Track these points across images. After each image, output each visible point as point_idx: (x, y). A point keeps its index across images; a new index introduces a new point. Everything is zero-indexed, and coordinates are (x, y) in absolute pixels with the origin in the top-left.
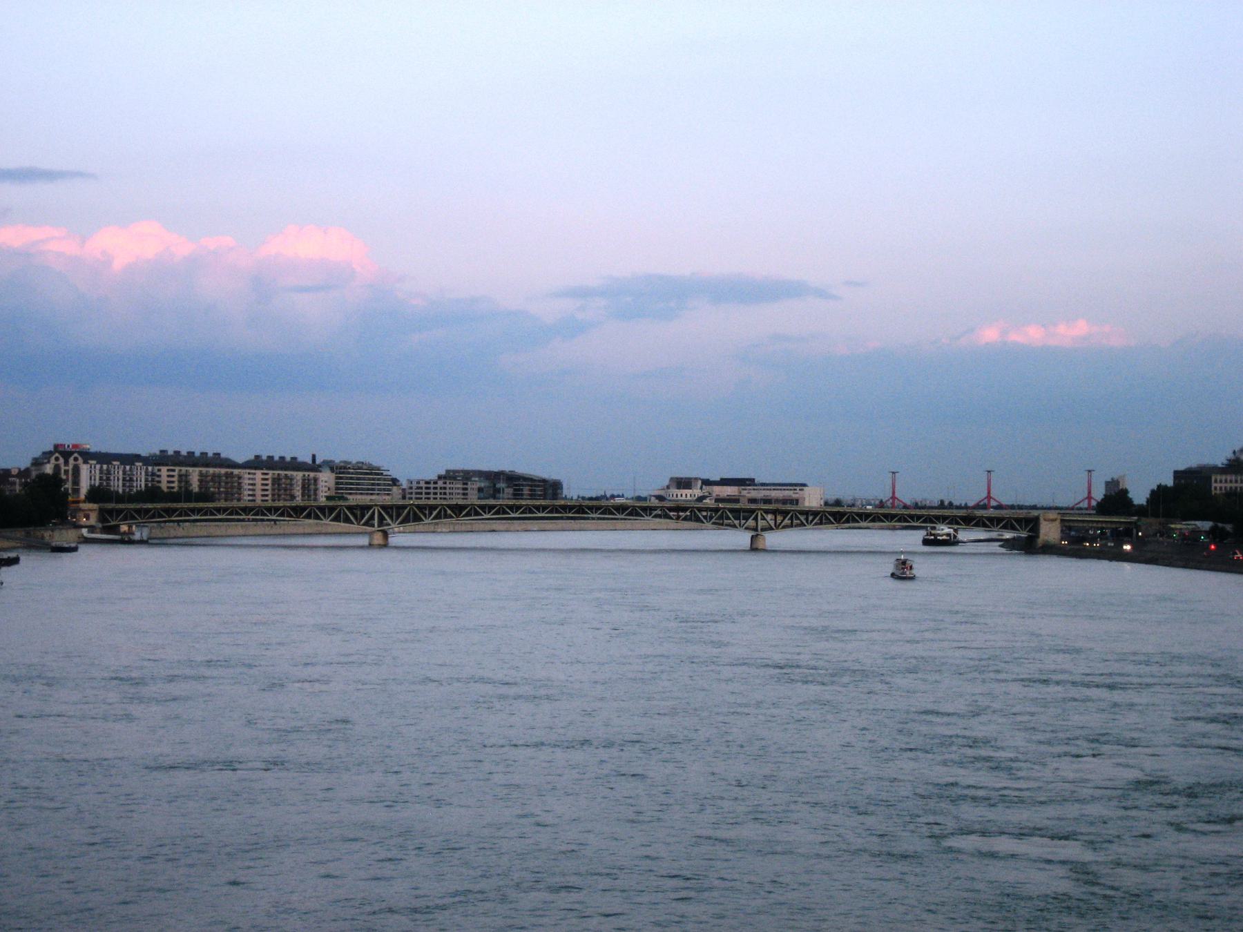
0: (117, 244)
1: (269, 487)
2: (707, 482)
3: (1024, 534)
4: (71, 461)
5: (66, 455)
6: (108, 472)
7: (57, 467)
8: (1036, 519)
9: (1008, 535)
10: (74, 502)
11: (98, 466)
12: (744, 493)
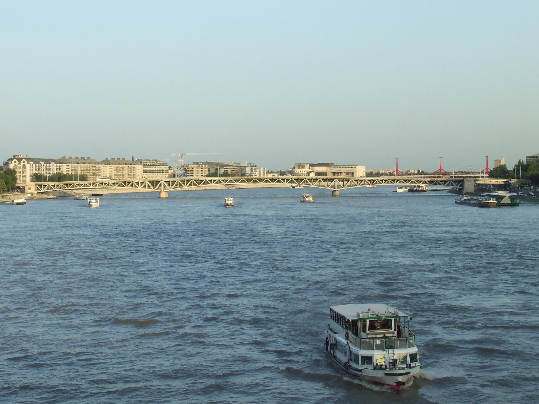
2: (311, 165)
3: (457, 187)
4: (22, 163)
5: (20, 160)
6: (39, 167)
8: (463, 180)
9: (449, 188)
10: (497, 173)
11: (34, 165)
12: (329, 169)
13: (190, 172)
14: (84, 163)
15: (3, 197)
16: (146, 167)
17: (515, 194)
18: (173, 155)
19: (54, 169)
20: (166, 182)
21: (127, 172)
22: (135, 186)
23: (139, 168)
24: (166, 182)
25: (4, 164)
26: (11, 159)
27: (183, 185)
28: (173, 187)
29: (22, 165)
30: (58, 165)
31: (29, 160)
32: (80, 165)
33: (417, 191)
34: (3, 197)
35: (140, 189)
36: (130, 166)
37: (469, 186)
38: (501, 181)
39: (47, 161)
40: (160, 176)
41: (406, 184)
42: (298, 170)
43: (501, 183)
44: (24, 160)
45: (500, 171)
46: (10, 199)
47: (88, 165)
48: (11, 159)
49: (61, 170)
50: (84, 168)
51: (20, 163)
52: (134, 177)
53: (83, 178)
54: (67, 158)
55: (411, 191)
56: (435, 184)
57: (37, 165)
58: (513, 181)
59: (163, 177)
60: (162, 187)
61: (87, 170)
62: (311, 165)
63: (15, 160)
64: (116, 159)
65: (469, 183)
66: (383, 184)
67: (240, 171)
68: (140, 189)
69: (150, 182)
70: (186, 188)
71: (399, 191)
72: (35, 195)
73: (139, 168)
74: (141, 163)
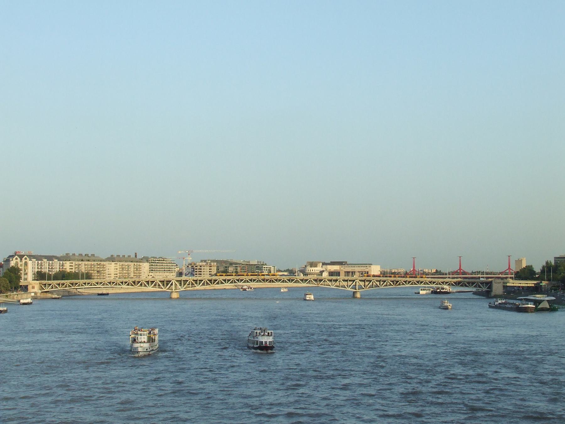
0: (564, 311)
1: (73, 267)
3: (485, 289)
4: (24, 260)
5: (21, 257)
6: (41, 264)
7: (17, 263)
8: (491, 282)
9: (474, 290)
11: (36, 262)
12: (342, 268)
13: (198, 270)
14: (88, 261)
15: (7, 296)
16: (152, 265)
17: (553, 298)
18: (180, 252)
19: (56, 267)
20: (177, 281)
21: (132, 269)
22: (145, 286)
23: (145, 266)
24: (177, 281)
25: (4, 261)
26: (12, 256)
27: (196, 285)
28: (185, 286)
29: (23, 262)
30: (61, 262)
31: (31, 257)
32: (84, 262)
33: (440, 293)
34: (7, 296)
35: (150, 288)
36: (136, 263)
37: (497, 288)
38: (531, 283)
39: (50, 258)
40: (167, 274)
41: (431, 285)
42: (309, 269)
43: (531, 285)
44: (26, 257)
45: (526, 273)
46: (13, 298)
47: (93, 263)
48: (12, 256)
49: (64, 267)
50: (87, 265)
51: (21, 260)
52: (140, 276)
53: (88, 276)
54: (71, 254)
55: (434, 292)
56: (462, 286)
57: (40, 262)
58: (544, 283)
59: (172, 276)
60: (173, 286)
61: (91, 267)
62: (324, 264)
63: (16, 257)
64: (121, 256)
65: (498, 285)
66: (407, 286)
67: (254, 270)
68: (150, 288)
69: (160, 281)
70: (198, 287)
71: (421, 292)
72: (39, 295)
73: (145, 266)
74: (147, 261)
